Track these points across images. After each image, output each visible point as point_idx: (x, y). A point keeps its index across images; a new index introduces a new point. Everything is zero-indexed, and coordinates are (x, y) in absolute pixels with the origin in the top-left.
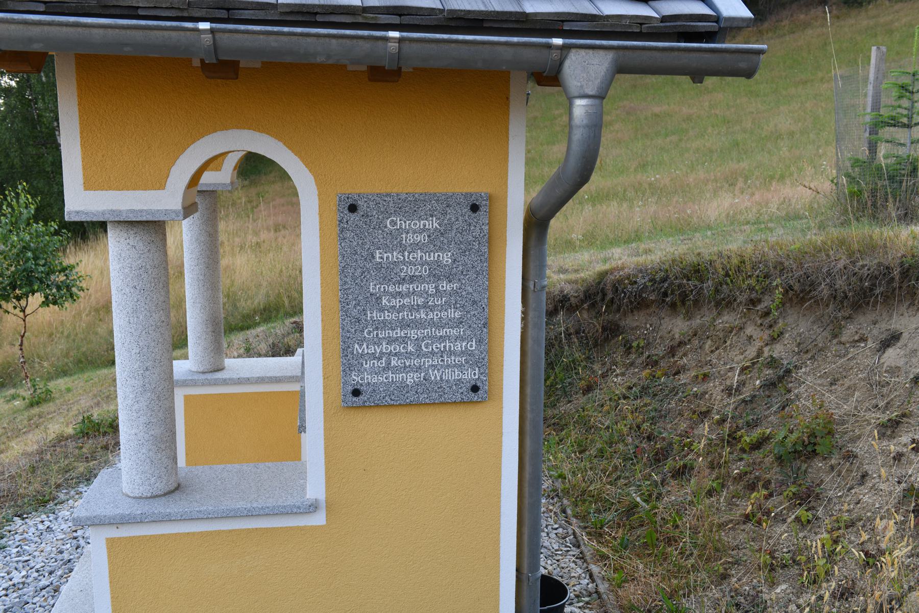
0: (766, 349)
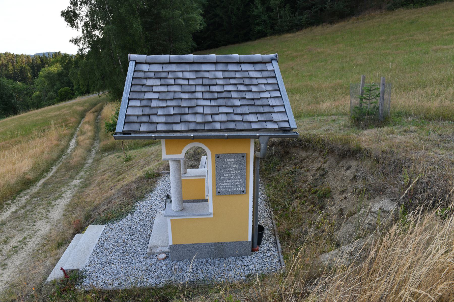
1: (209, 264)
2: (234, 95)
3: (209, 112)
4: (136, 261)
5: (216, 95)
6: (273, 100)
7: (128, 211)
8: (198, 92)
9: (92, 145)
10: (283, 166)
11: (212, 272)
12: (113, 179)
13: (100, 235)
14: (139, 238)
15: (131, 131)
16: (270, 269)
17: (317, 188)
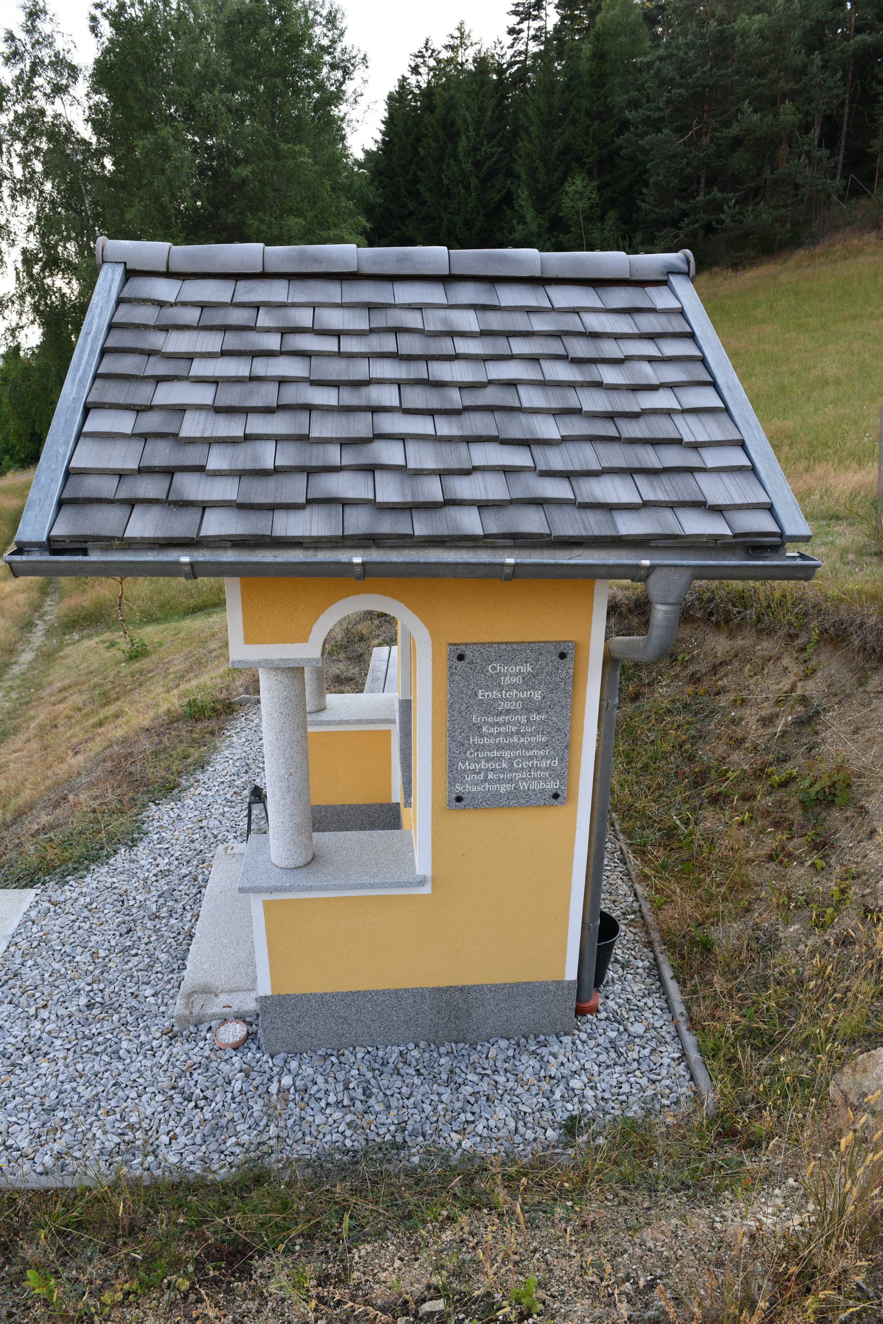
0: (799, 684)
1: (412, 1071)
2: (530, 398)
3: (431, 465)
4: (133, 1047)
5: (455, 398)
6: (691, 419)
7: (119, 837)
8: (381, 382)
9: (37, 607)
10: (650, 685)
11: (428, 1109)
12: (87, 716)
13: (11, 930)
14: (150, 946)
15: (86, 539)
16: (649, 1092)
17: (791, 769)
